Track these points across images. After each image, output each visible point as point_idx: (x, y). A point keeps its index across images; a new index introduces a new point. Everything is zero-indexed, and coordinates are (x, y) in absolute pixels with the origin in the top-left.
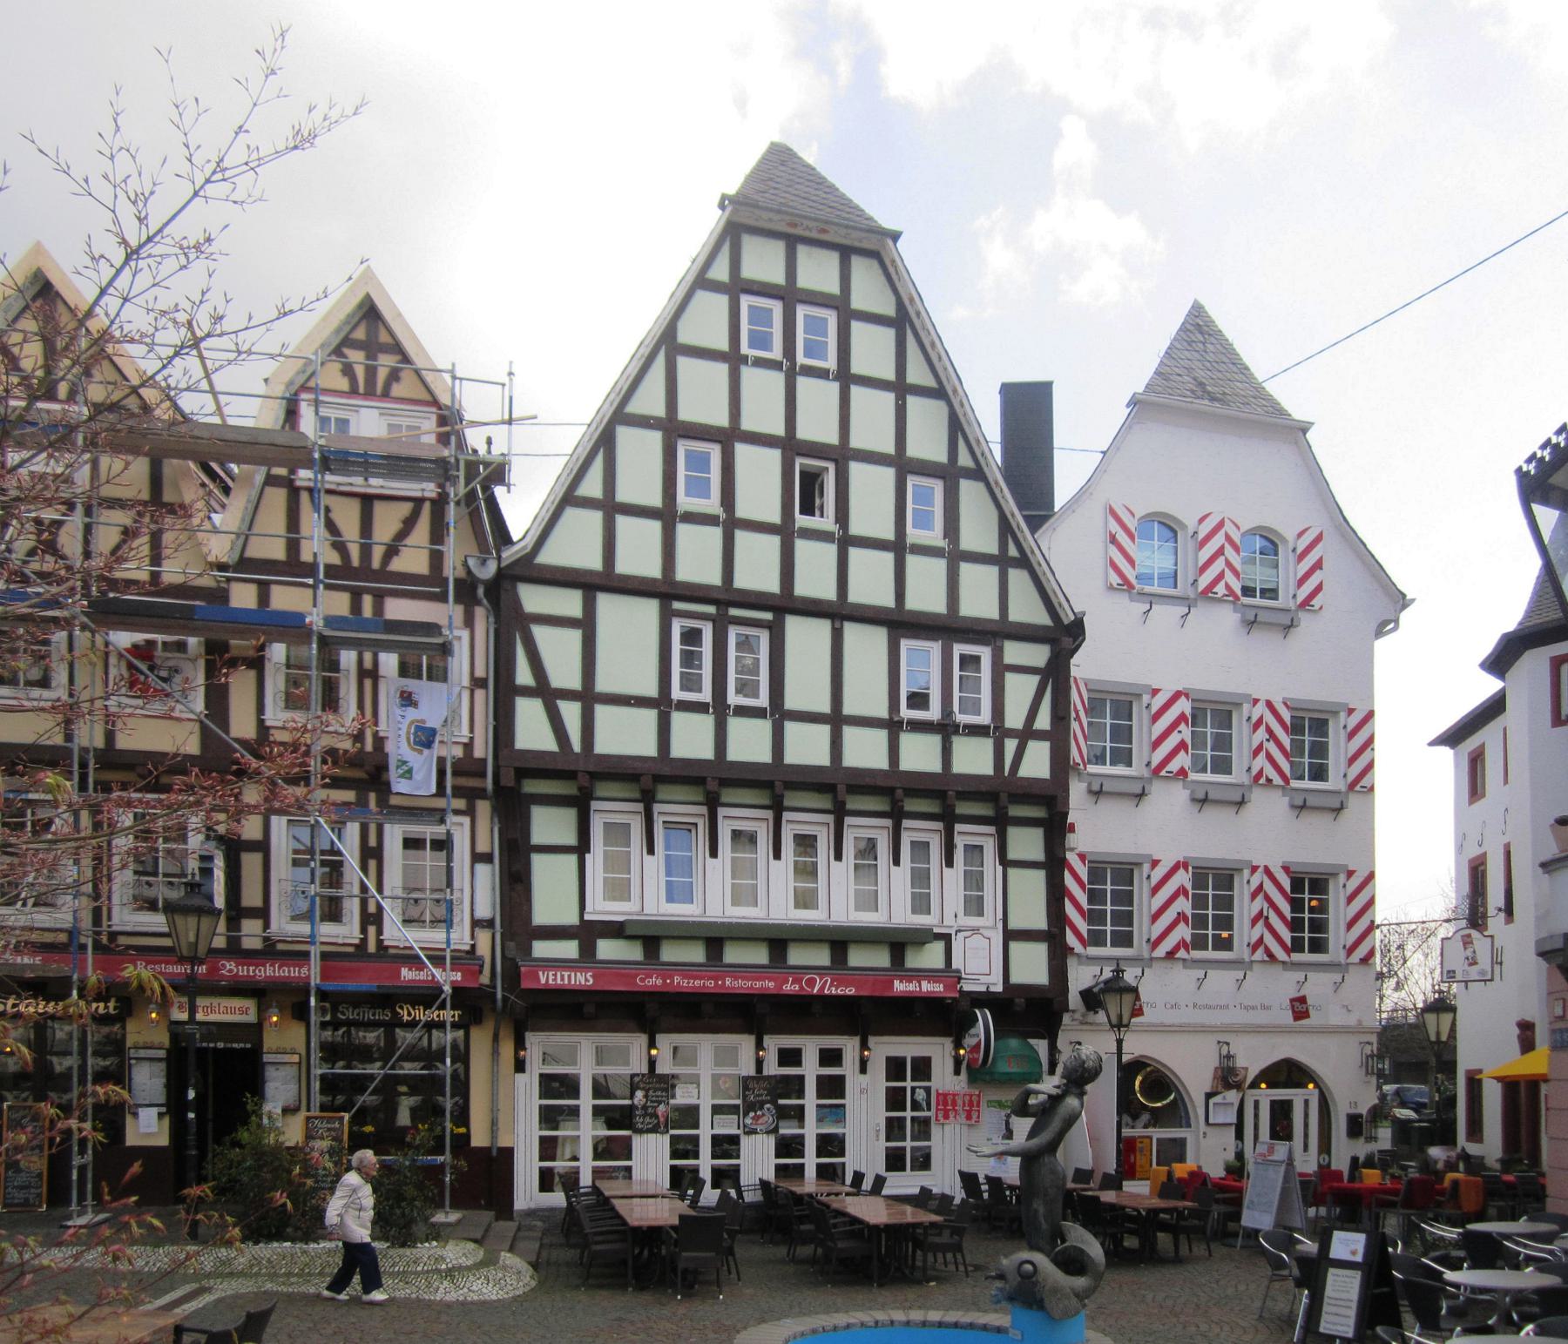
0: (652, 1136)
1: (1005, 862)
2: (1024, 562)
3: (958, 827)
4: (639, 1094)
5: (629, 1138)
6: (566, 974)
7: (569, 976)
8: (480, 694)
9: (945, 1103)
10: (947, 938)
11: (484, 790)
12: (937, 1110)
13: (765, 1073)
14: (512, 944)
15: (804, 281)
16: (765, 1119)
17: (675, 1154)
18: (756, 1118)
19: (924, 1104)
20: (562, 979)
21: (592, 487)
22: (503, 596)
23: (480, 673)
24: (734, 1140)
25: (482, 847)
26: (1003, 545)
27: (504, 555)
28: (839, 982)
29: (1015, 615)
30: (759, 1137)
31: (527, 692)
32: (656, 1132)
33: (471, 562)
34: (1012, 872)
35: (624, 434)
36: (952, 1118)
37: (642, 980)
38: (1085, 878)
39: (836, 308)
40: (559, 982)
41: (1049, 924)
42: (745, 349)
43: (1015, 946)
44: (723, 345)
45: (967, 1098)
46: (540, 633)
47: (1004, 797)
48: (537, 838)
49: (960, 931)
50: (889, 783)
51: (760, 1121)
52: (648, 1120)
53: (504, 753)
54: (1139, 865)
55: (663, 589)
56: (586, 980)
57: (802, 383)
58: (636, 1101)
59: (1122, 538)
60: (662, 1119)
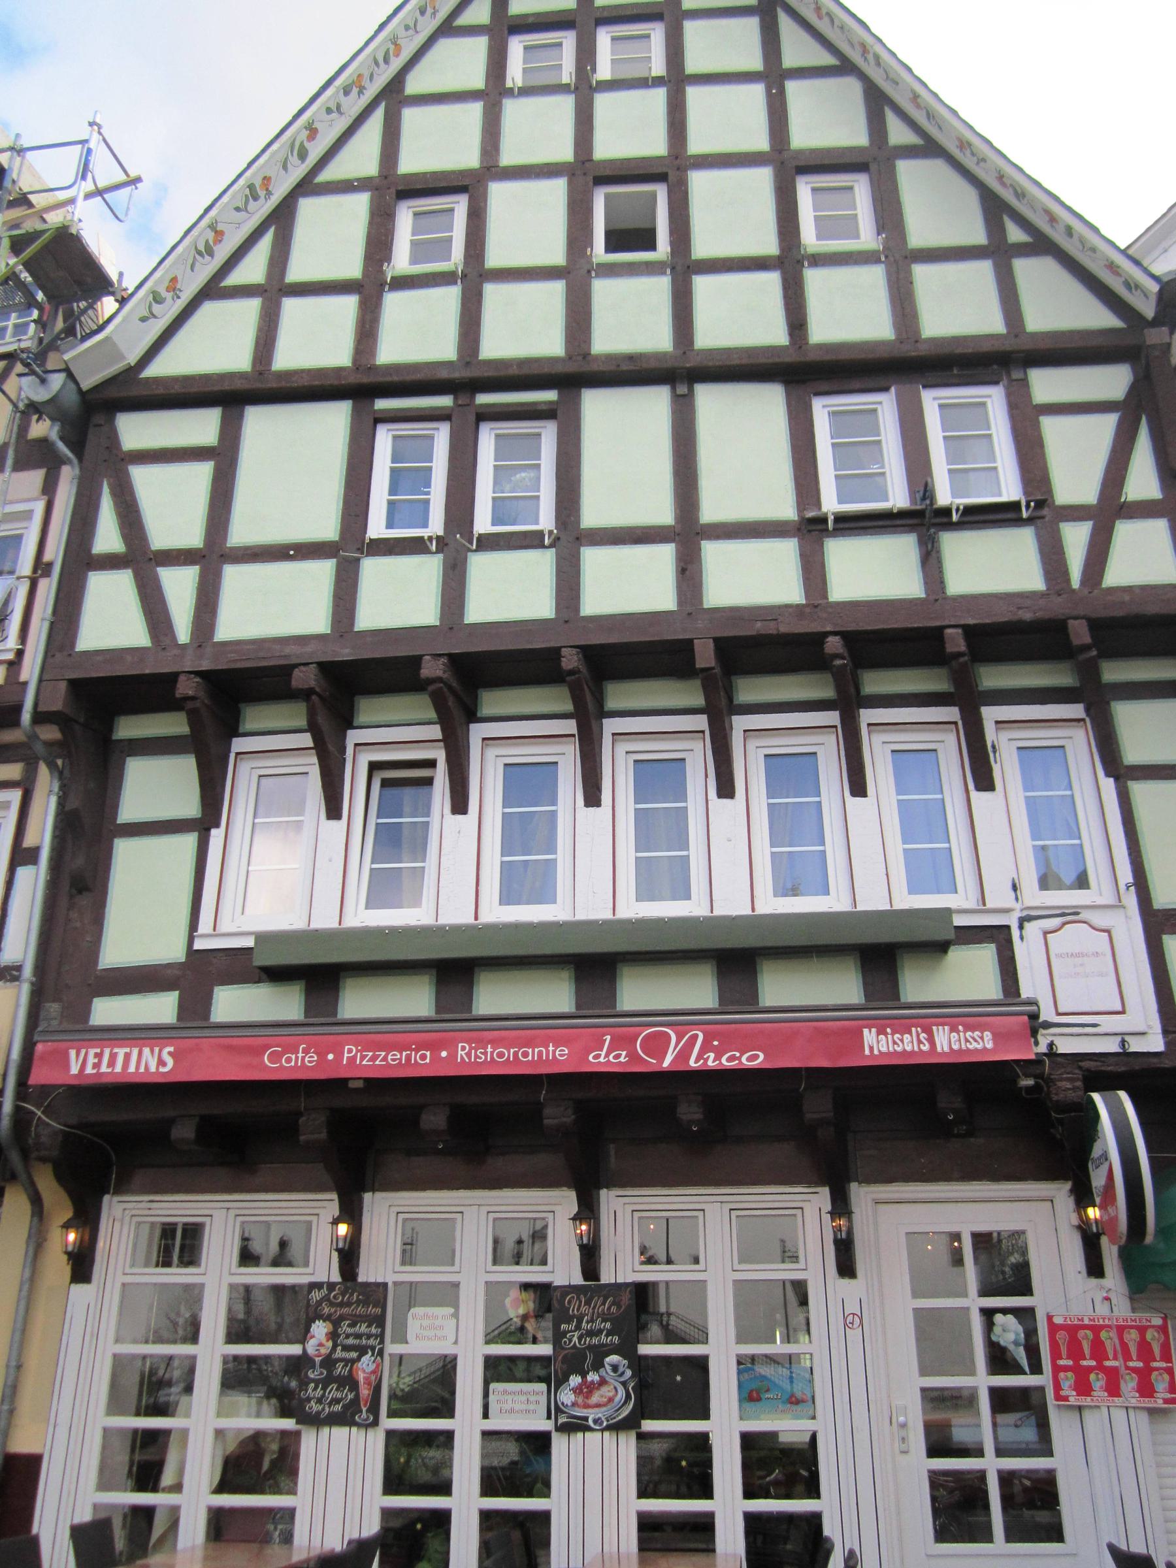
0: (340, 1433)
2: (1041, 245)
4: (320, 1330)
6: (121, 1052)
7: (127, 1057)
9: (1076, 1352)
10: (1000, 937)
12: (1057, 1369)
13: (607, 1276)
16: (606, 1391)
17: (394, 1482)
18: (585, 1390)
19: (1021, 1355)
20: (112, 1063)
21: (253, 269)
24: (538, 1443)
28: (719, 1039)
30: (593, 1438)
32: (351, 1423)
34: (1139, 790)
36: (1099, 1393)
37: (275, 1057)
45: (1132, 1337)
46: (142, 477)
49: (1030, 919)
51: (595, 1398)
52: (333, 1392)
55: (353, 379)
56: (161, 1063)
58: (311, 1347)
60: (365, 1392)
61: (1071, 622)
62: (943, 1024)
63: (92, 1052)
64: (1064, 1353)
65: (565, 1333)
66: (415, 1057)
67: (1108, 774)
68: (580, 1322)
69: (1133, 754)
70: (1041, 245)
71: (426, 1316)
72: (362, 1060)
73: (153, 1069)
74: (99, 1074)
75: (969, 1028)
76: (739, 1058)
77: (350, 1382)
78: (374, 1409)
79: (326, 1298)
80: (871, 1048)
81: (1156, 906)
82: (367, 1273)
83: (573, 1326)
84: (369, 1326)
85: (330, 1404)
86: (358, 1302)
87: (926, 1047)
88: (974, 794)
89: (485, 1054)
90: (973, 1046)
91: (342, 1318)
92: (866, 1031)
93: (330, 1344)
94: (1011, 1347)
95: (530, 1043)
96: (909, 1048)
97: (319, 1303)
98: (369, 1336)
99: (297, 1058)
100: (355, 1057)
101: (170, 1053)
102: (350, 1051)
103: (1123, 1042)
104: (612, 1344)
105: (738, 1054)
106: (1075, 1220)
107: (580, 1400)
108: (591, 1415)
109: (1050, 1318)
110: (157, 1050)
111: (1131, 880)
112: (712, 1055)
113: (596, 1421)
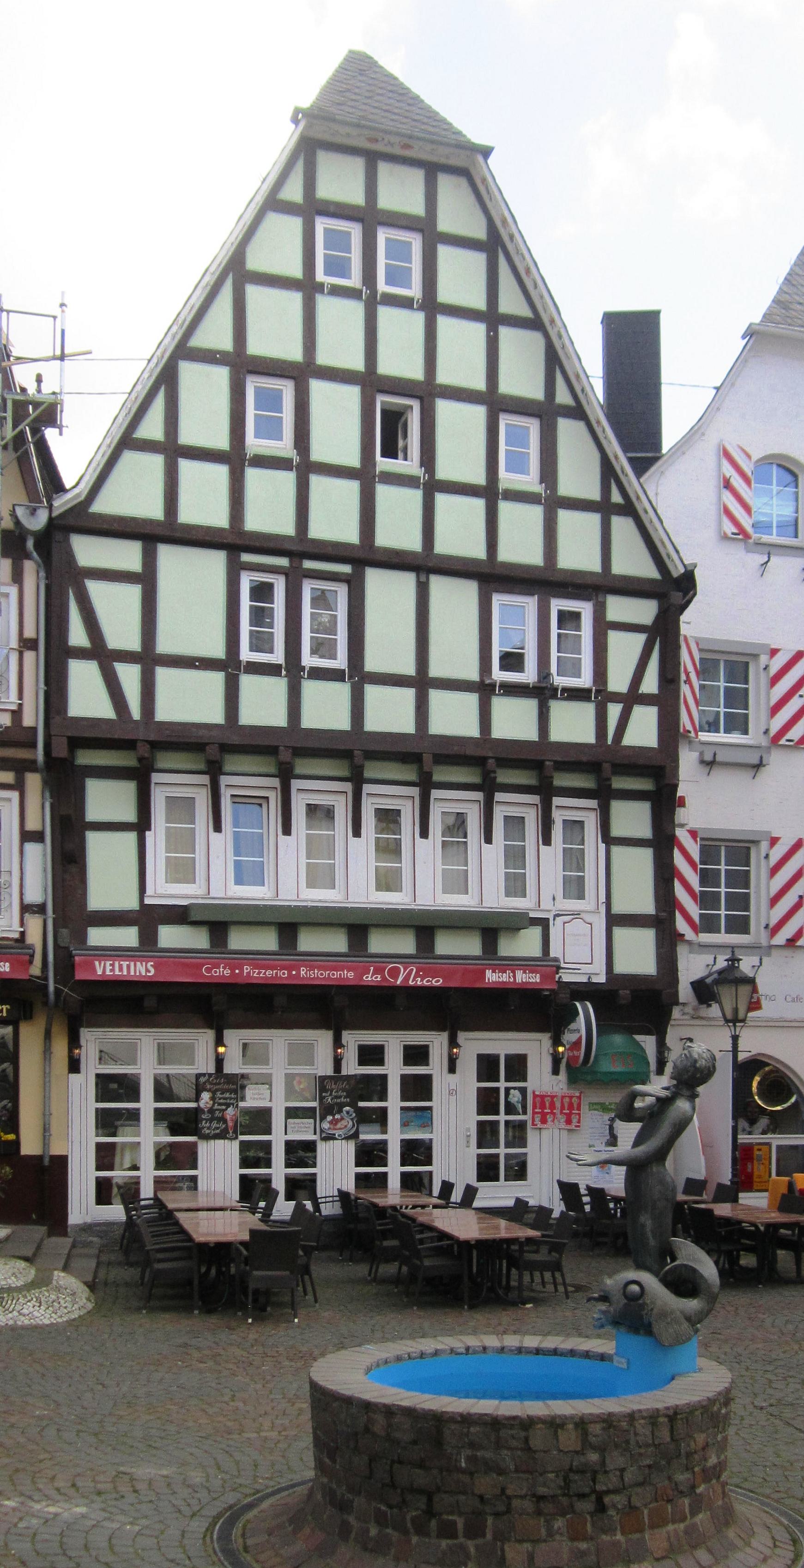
0: (220, 1143)
1: (609, 840)
3: (557, 801)
4: (206, 1096)
5: (194, 1145)
6: (125, 964)
7: (128, 967)
9: (543, 1106)
10: (544, 924)
12: (534, 1113)
13: (344, 1072)
14: (64, 932)
15: (386, 201)
16: (344, 1123)
17: (245, 1162)
18: (334, 1122)
19: (519, 1107)
20: (121, 969)
24: (310, 1147)
25: (32, 825)
29: (619, 568)
31: (81, 654)
34: (616, 850)
36: (549, 1123)
37: (209, 970)
40: (117, 972)
42: (320, 276)
45: (567, 1100)
46: (94, 587)
48: (93, 813)
50: (479, 753)
51: (339, 1126)
52: (215, 1124)
53: (56, 720)
55: (230, 540)
56: (147, 971)
58: (202, 1104)
60: (230, 1124)
61: (604, 764)
63: (108, 963)
64: (538, 1105)
66: (280, 973)
67: (603, 842)
68: (332, 1092)
69: (616, 831)
71: (255, 1089)
74: (114, 975)
75: (531, 972)
76: (431, 981)
77: (223, 1120)
78: (235, 1132)
80: (489, 979)
82: (228, 1069)
84: (230, 1094)
85: (214, 1130)
86: (224, 1083)
87: (512, 980)
89: (314, 973)
90: (531, 980)
91: (217, 1090)
92: (487, 971)
93: (211, 1102)
94: (516, 1104)
96: (505, 980)
97: (205, 1083)
98: (231, 1099)
101: (151, 965)
102: (247, 969)
103: (589, 978)
104: (347, 1102)
106: (551, 1051)
108: (337, 1133)
109: (534, 1092)
110: (144, 963)
112: (419, 979)
113: (339, 1136)
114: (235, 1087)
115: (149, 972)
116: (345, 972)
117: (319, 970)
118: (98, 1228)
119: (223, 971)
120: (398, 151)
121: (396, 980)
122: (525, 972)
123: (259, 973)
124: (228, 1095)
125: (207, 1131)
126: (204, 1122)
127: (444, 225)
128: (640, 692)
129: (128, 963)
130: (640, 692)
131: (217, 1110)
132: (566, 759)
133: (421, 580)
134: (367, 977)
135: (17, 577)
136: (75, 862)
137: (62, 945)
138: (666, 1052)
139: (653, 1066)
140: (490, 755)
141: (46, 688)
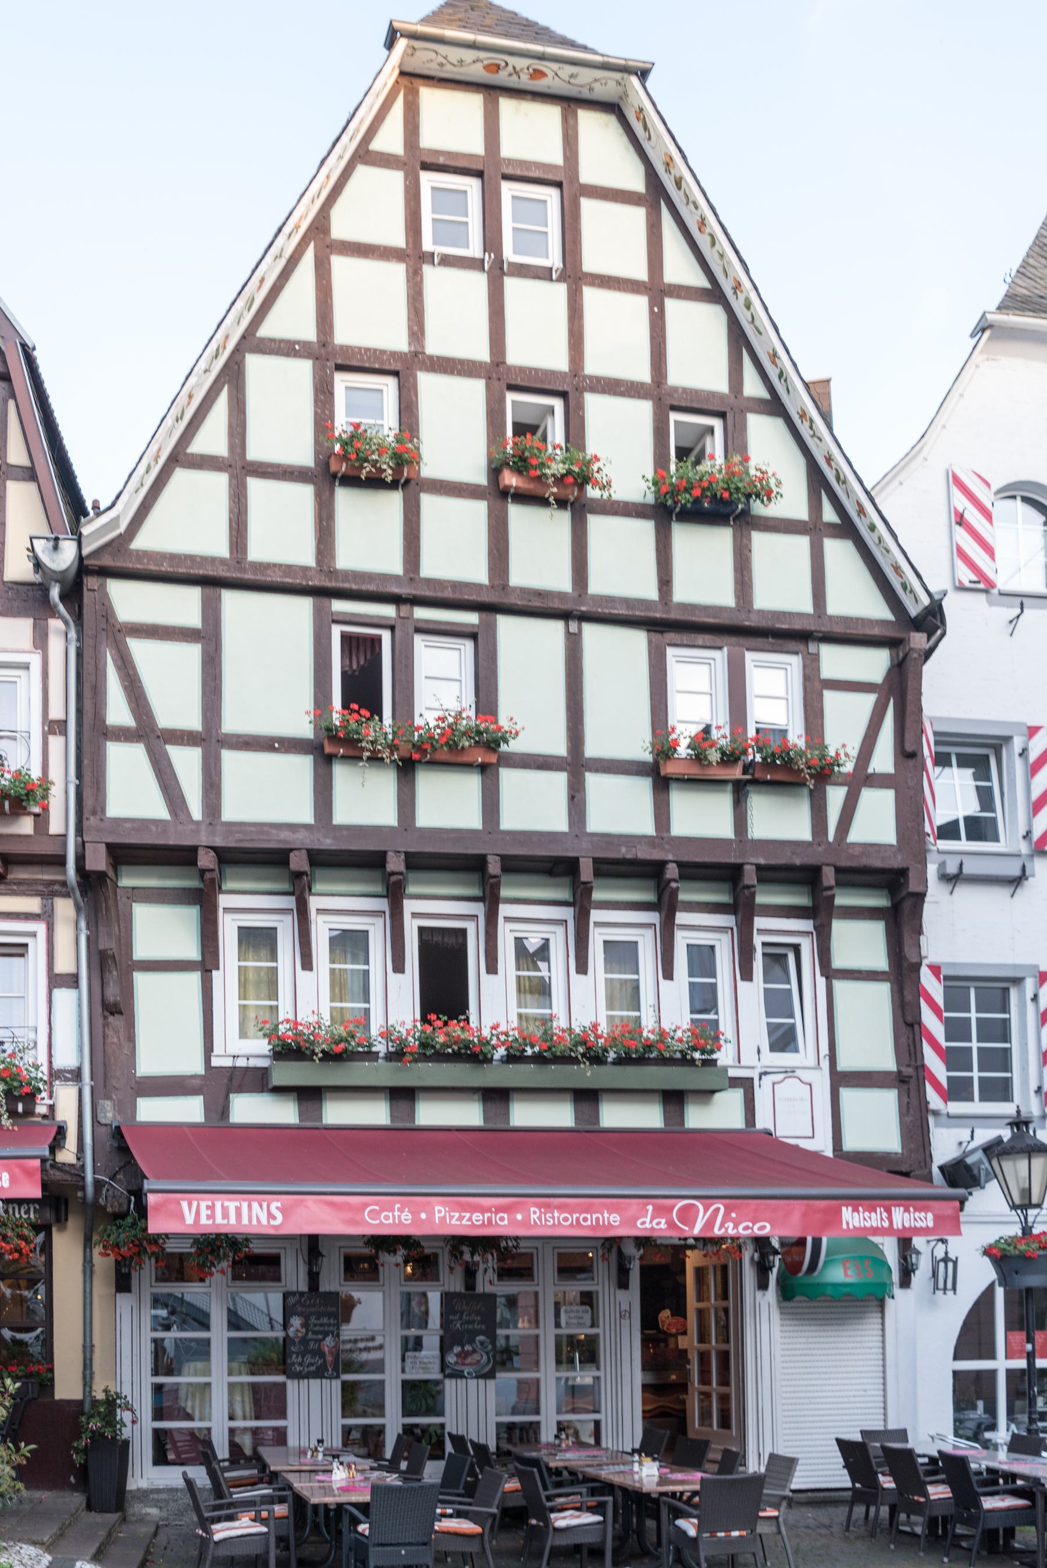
0: (315, 1383)
1: (829, 972)
2: (847, 529)
3: (759, 922)
4: (296, 1322)
5: (283, 1386)
6: (232, 1205)
7: (238, 1210)
8: (56, 743)
10: (746, 1085)
11: (64, 884)
15: (510, 148)
16: (476, 1357)
17: (348, 1408)
18: (463, 1355)
20: (225, 1215)
22: (87, 598)
23: (56, 712)
25: (64, 965)
26: (815, 506)
27: (86, 531)
29: (836, 607)
31: (123, 735)
32: (322, 1377)
33: (39, 546)
34: (838, 985)
35: (254, 364)
38: (940, 1001)
39: (559, 185)
40: (219, 1220)
41: (898, 1062)
42: (428, 244)
43: (847, 1094)
44: (398, 239)
46: (139, 648)
47: (829, 876)
48: (141, 951)
49: (766, 1073)
50: (656, 855)
51: (469, 1360)
52: (308, 1359)
53: (91, 822)
54: (1018, 981)
55: (314, 582)
56: (271, 1216)
57: (511, 284)
58: (291, 1332)
59: (973, 516)
60: (329, 1358)
62: (899, 1206)
63: (203, 1205)
65: (452, 1321)
66: (496, 1218)
67: (822, 975)
69: (839, 961)
70: (847, 529)
72: (451, 1220)
73: (264, 1222)
76: (752, 1228)
79: (299, 1302)
80: (848, 1224)
81: (839, 1069)
82: (325, 1286)
83: (457, 1317)
88: (740, 983)
89: (553, 1218)
91: (311, 1314)
92: (844, 1209)
93: (304, 1330)
95: (588, 1210)
96: (875, 1225)
97: (294, 1305)
98: (329, 1325)
99: (394, 1216)
100: (445, 1217)
101: (277, 1208)
102: (440, 1212)
105: (751, 1225)
107: (460, 1361)
110: (265, 1205)
111: (827, 1052)
114: (334, 1309)
115: (274, 1218)
116: (606, 1215)
117: (561, 1212)
118: (156, 1496)
119: (399, 1217)
120: (525, 81)
121: (692, 1227)
122: (907, 1210)
123: (461, 1218)
124: (325, 1320)
125: (298, 1369)
126: (294, 1356)
127: (587, 175)
128: (870, 770)
129: (238, 1204)
130: (870, 770)
131: (312, 1340)
132: (773, 862)
133: (571, 630)
134: (643, 1223)
135: (41, 641)
136: (120, 1013)
137: (103, 1121)
138: (914, 1256)
139: (896, 1277)
140: (670, 857)
141: (78, 782)
